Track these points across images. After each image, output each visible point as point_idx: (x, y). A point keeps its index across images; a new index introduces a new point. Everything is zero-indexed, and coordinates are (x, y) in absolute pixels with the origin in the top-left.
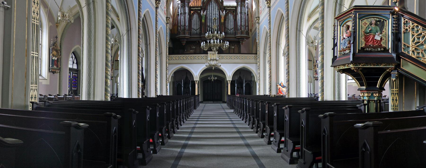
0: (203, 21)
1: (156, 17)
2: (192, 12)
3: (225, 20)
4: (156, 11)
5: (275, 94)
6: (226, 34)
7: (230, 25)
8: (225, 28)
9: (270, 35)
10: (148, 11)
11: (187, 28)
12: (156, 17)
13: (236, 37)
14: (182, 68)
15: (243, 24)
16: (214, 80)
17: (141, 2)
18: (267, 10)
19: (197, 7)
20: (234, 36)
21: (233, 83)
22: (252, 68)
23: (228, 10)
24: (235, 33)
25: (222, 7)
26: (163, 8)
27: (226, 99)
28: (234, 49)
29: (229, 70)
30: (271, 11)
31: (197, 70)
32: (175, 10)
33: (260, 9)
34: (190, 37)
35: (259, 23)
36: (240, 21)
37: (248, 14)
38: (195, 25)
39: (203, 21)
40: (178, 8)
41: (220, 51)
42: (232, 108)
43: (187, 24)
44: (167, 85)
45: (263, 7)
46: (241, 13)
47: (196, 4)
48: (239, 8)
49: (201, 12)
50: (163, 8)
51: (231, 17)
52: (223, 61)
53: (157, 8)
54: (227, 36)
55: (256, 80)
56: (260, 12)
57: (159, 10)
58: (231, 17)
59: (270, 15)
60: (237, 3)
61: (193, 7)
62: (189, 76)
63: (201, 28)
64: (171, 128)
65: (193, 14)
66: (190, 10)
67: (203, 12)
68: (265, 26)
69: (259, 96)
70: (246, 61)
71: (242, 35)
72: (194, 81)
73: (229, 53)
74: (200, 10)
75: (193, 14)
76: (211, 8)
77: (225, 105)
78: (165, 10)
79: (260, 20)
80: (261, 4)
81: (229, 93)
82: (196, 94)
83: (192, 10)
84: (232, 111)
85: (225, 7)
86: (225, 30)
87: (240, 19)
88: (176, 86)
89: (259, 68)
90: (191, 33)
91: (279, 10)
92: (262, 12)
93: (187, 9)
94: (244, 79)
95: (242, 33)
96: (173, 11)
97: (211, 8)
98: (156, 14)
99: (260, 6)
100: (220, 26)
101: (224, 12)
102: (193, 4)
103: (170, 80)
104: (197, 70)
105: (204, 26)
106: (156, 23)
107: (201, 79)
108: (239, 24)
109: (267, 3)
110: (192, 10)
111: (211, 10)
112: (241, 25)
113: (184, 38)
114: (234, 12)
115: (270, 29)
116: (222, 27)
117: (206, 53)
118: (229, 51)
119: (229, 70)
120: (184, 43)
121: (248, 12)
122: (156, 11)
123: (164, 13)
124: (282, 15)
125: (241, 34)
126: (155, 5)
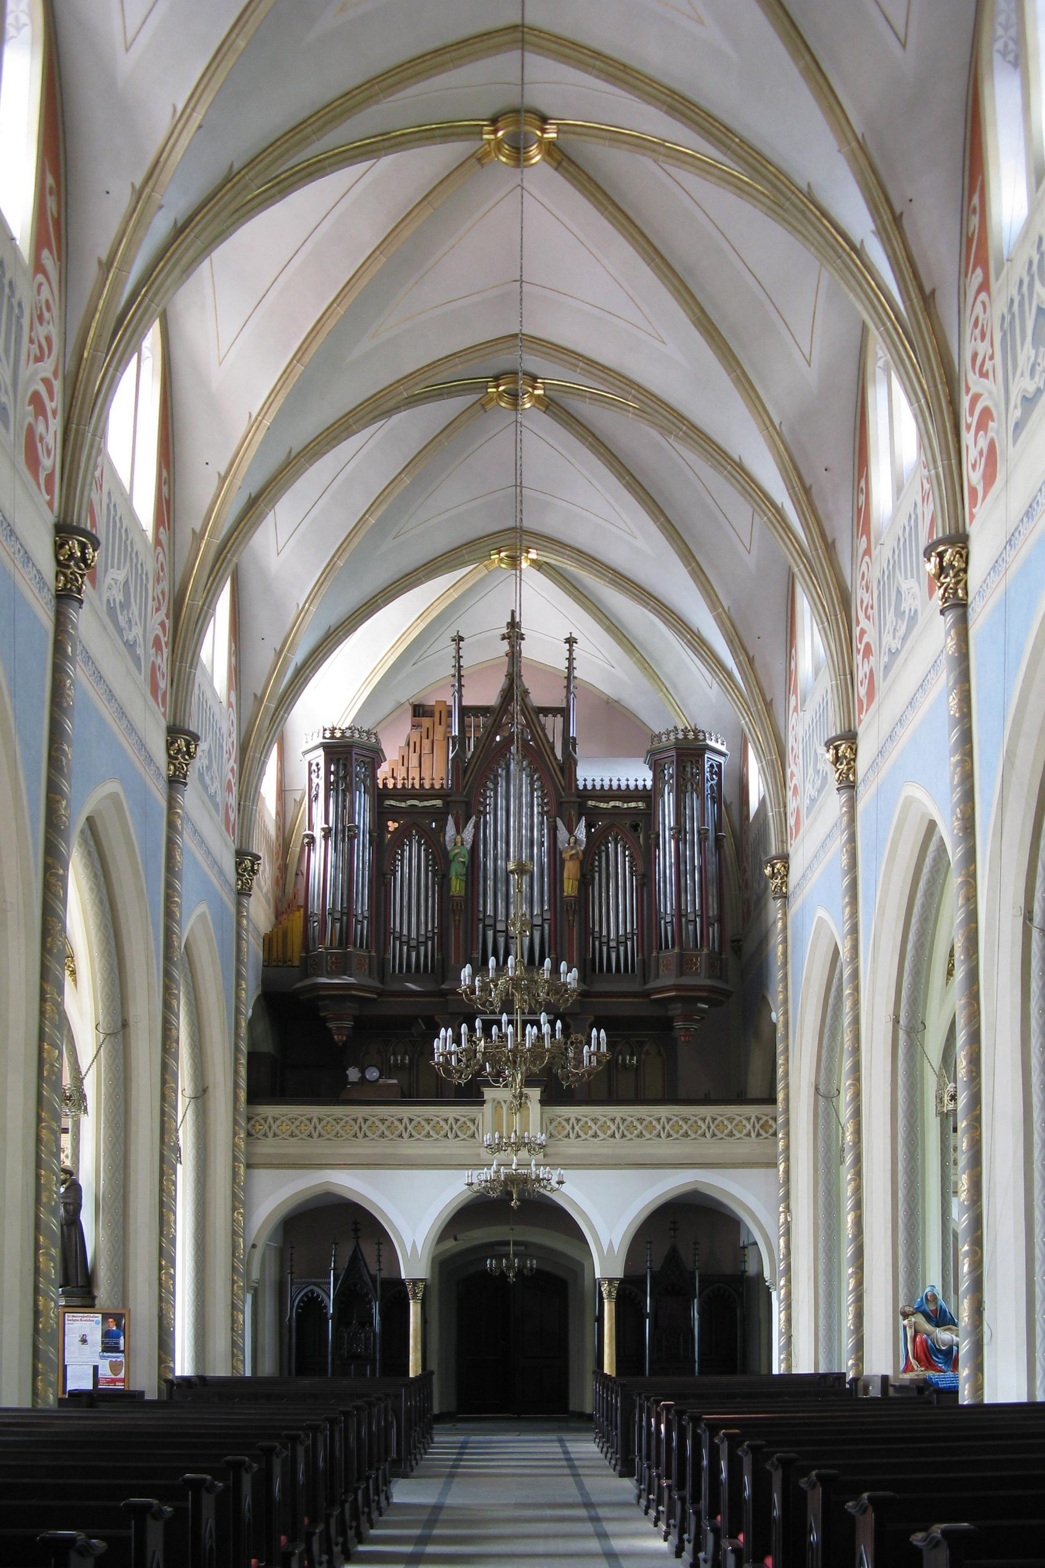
0: (457, 887)
1: (171, 843)
2: (392, 826)
3: (585, 881)
4: (172, 804)
5: (889, 1372)
6: (588, 970)
7: (616, 915)
8: (586, 931)
9: (855, 975)
10: (114, 797)
11: (362, 929)
12: (171, 843)
13: (646, 994)
14: (328, 1194)
15: (692, 903)
16: (519, 1273)
17: (68, 726)
18: (835, 802)
19: (423, 794)
20: (636, 987)
21: (628, 1292)
22: (743, 1191)
23: (605, 813)
24: (645, 964)
25: (567, 800)
26: (215, 787)
27: (586, 1397)
28: (637, 1069)
29: (607, 1208)
30: (861, 806)
31: (415, 1207)
32: (249, 703)
33: (791, 806)
34: (381, 994)
35: (785, 897)
36: (670, 889)
37: (718, 840)
38: (413, 916)
39: (457, 887)
40: (313, 799)
41: (557, 1092)
42: (626, 1470)
43: (362, 906)
44: (234, 1307)
45: (810, 790)
46: (679, 832)
47: (414, 773)
48: (669, 801)
49: (442, 828)
50: (215, 787)
51: (619, 860)
52: (571, 1148)
53: (175, 782)
54: (599, 987)
55: (767, 1274)
56: (791, 821)
57: (190, 798)
58: (619, 860)
59: (852, 839)
60: (657, 768)
61: (403, 794)
62: (368, 1251)
63: (443, 933)
64: (392, 1423)
65: (402, 835)
66: (380, 814)
67: (458, 831)
68: (821, 913)
69: (790, 1380)
70: (712, 1149)
71: (685, 981)
72: (402, 1283)
73: (611, 1099)
74: (440, 816)
75: (402, 835)
76: (501, 802)
77: (586, 1448)
78: (233, 801)
79: (793, 878)
80: (795, 769)
81: (609, 1367)
82: (414, 1370)
83: (395, 814)
84: (629, 1484)
85: (587, 794)
86: (584, 947)
87: (670, 873)
88: (291, 1312)
89: (787, 1196)
90: (383, 963)
91: (909, 801)
92: (805, 823)
93: (362, 803)
94: (698, 1267)
95: (683, 965)
96: (281, 812)
97: (501, 802)
98: (171, 825)
99: (790, 784)
100: (554, 922)
101: (581, 832)
102: (401, 773)
103: (255, 1275)
104: (415, 1207)
105: (462, 923)
106: (169, 885)
107: (446, 1265)
108: (667, 906)
109: (837, 760)
110: (395, 814)
111: (501, 814)
112: (679, 913)
113: (342, 996)
114: (635, 827)
115: (854, 930)
116: (569, 924)
117: (470, 1094)
118: (609, 1088)
119: (607, 1208)
120: (340, 1029)
121: (718, 827)
122: (172, 804)
123: (220, 819)
124: (932, 825)
125: (681, 973)
126: (161, 757)
